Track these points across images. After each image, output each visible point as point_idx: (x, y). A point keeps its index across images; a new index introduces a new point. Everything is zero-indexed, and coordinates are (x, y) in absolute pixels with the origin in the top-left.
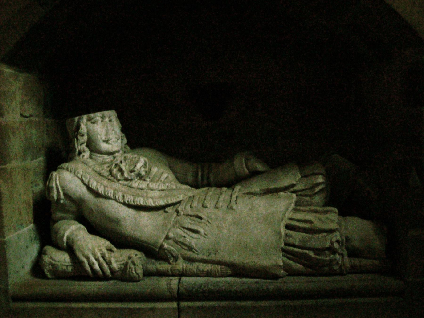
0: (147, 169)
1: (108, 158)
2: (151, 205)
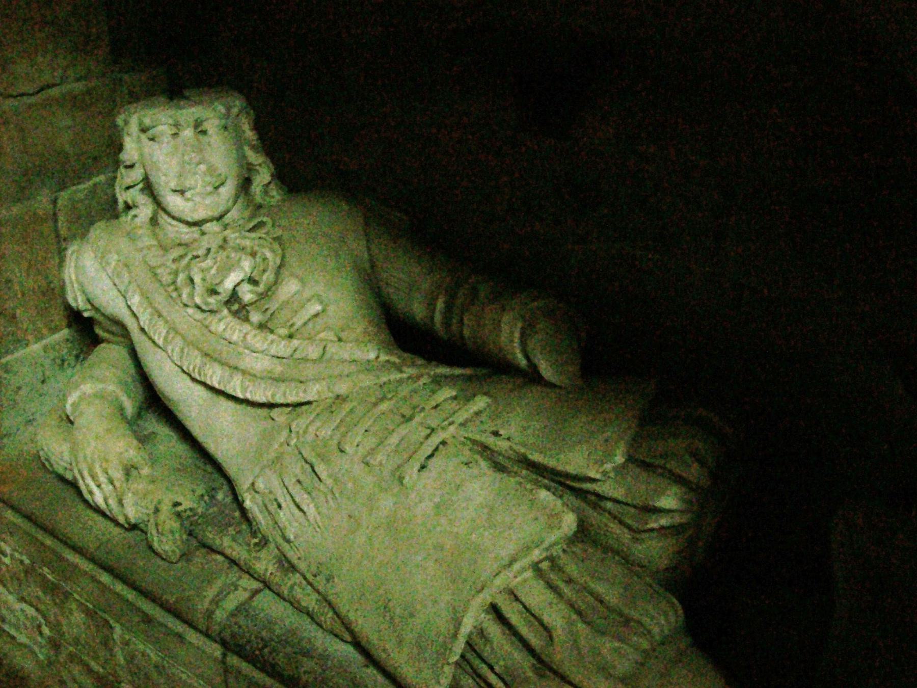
0: (261, 288)
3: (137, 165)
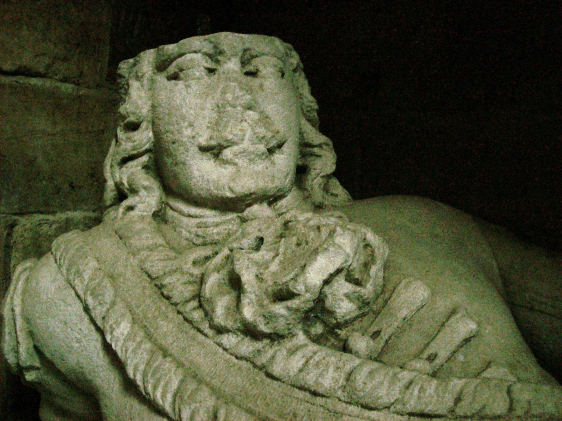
0: (368, 290)
1: (217, 225)
3: (144, 125)
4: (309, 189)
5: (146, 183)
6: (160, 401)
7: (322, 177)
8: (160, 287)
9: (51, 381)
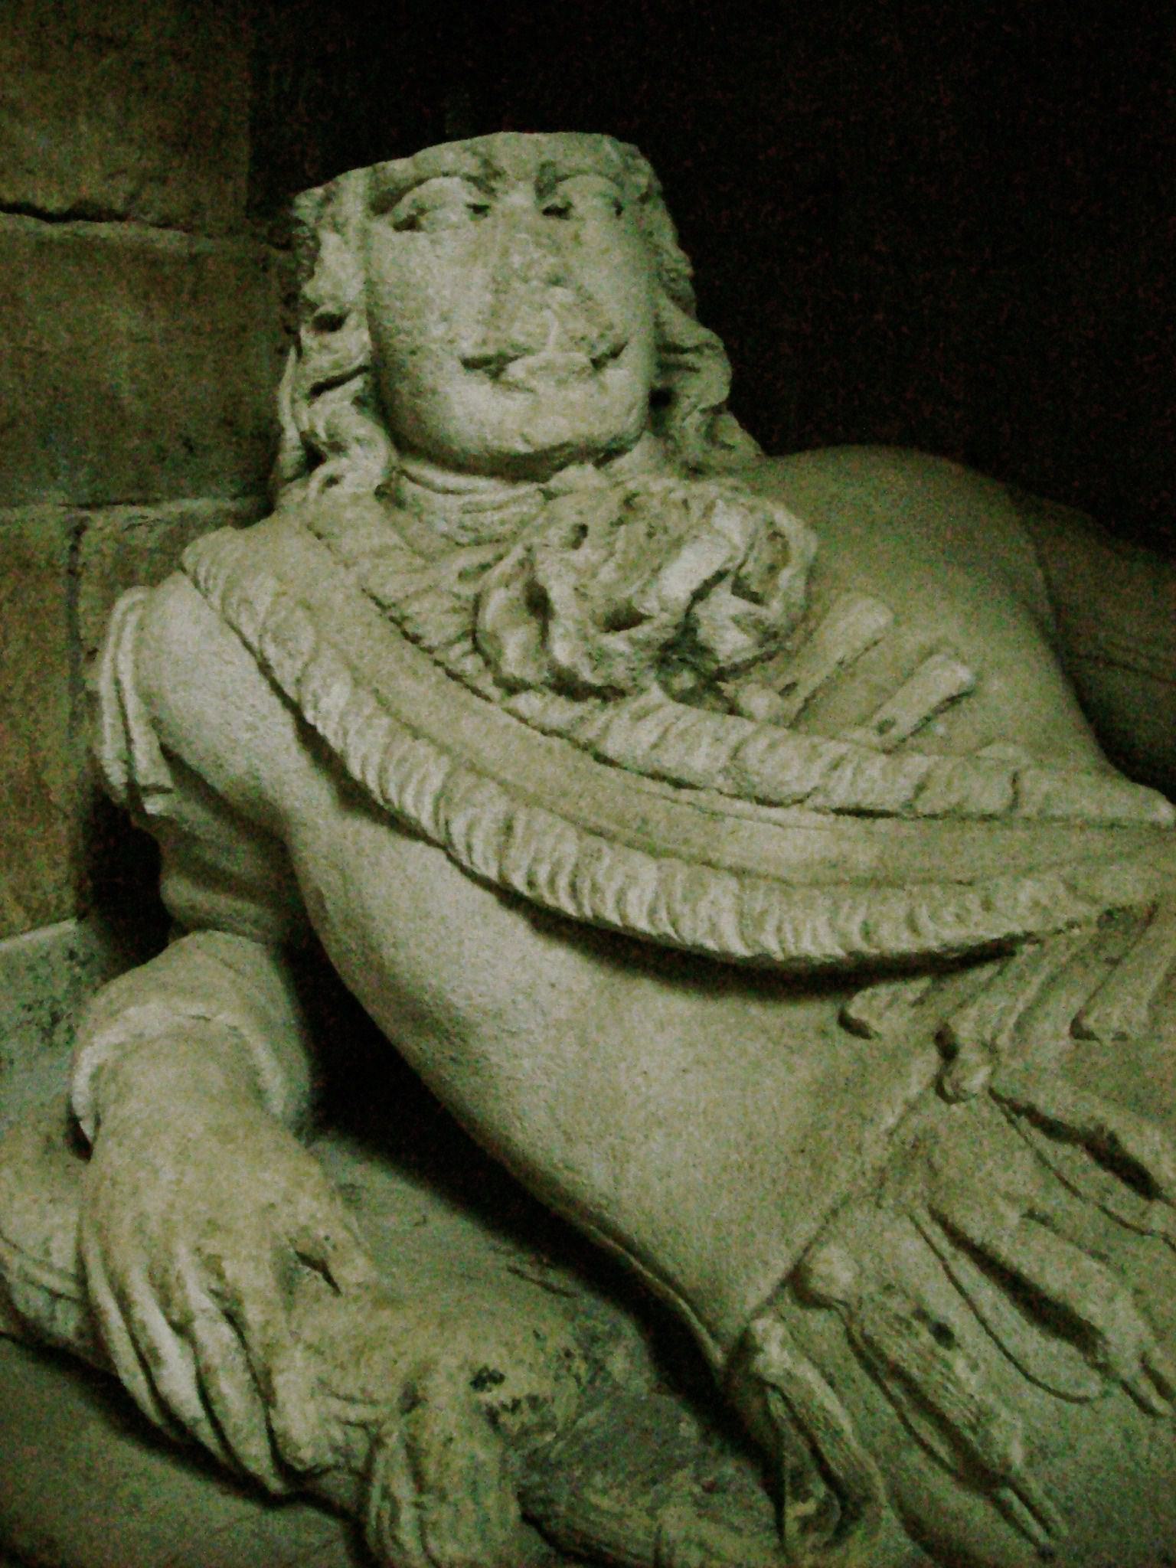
1: (499, 507)
2: (711, 945)
3: (352, 321)
4: (677, 435)
5: (362, 432)
6: (411, 810)
7: (703, 411)
8: (398, 622)
9: (195, 815)
